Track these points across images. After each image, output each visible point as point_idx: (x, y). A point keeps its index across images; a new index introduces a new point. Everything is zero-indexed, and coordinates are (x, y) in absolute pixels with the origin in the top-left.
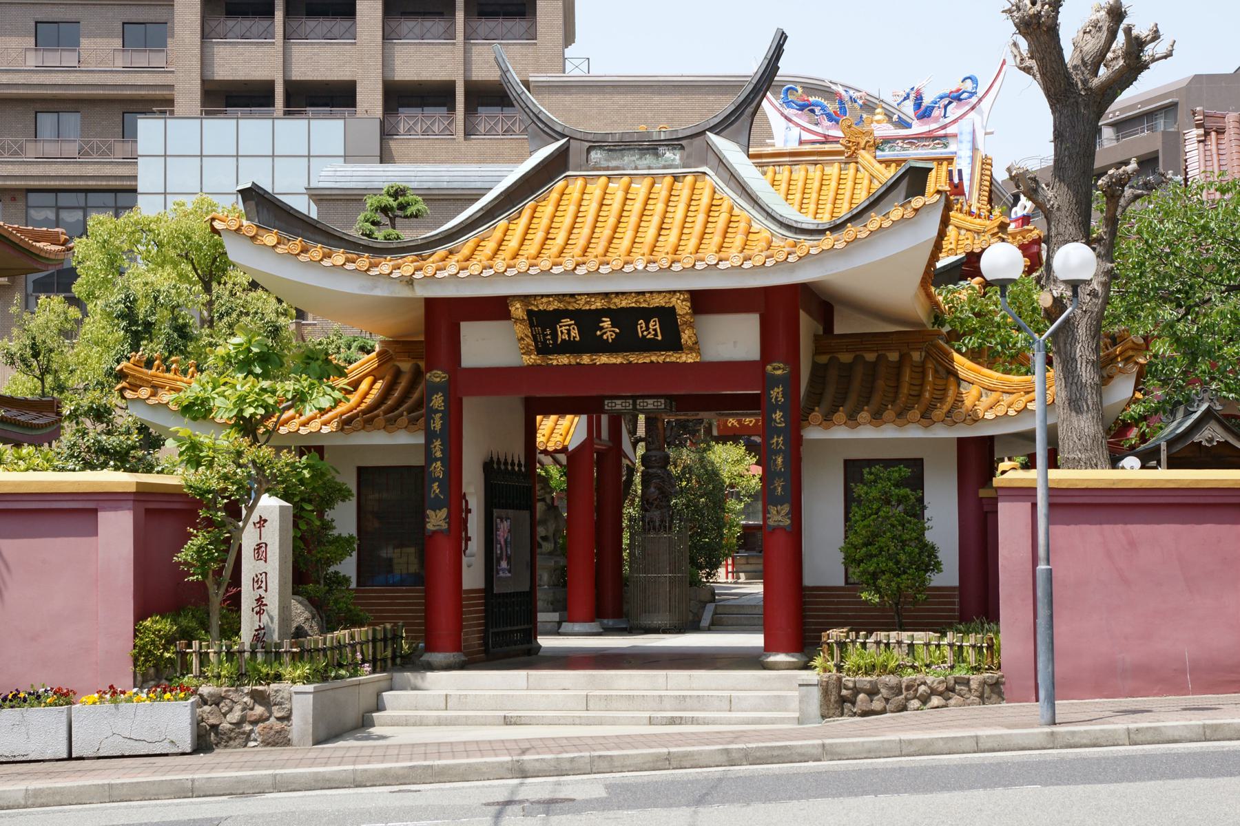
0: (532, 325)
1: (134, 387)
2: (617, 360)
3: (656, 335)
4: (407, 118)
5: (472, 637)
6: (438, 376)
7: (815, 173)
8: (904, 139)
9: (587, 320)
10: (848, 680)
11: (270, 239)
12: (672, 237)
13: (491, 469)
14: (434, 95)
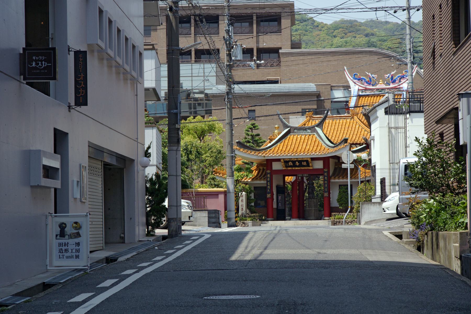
1: (216, 173)
5: (275, 215)
6: (268, 171)
7: (345, 121)
8: (388, 89)
9: (294, 162)
10: (335, 220)
11: (242, 150)
12: (308, 147)
13: (278, 187)
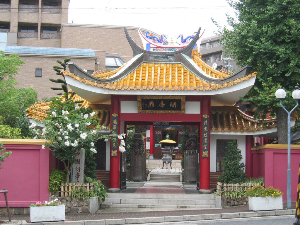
0: (142, 103)
2: (164, 112)
3: (175, 106)
4: (24, 33)
14: (32, 27)
